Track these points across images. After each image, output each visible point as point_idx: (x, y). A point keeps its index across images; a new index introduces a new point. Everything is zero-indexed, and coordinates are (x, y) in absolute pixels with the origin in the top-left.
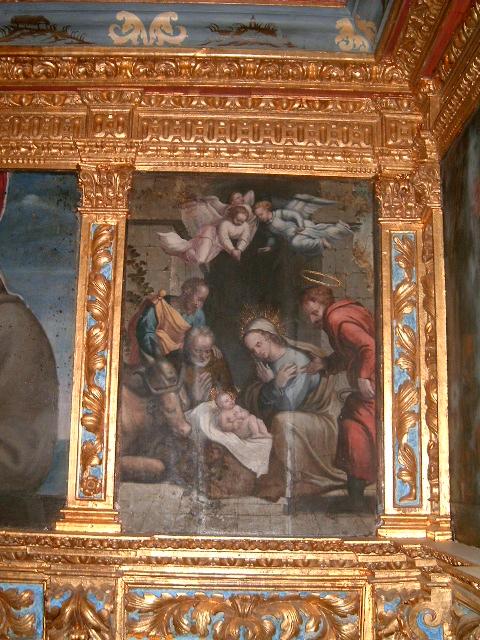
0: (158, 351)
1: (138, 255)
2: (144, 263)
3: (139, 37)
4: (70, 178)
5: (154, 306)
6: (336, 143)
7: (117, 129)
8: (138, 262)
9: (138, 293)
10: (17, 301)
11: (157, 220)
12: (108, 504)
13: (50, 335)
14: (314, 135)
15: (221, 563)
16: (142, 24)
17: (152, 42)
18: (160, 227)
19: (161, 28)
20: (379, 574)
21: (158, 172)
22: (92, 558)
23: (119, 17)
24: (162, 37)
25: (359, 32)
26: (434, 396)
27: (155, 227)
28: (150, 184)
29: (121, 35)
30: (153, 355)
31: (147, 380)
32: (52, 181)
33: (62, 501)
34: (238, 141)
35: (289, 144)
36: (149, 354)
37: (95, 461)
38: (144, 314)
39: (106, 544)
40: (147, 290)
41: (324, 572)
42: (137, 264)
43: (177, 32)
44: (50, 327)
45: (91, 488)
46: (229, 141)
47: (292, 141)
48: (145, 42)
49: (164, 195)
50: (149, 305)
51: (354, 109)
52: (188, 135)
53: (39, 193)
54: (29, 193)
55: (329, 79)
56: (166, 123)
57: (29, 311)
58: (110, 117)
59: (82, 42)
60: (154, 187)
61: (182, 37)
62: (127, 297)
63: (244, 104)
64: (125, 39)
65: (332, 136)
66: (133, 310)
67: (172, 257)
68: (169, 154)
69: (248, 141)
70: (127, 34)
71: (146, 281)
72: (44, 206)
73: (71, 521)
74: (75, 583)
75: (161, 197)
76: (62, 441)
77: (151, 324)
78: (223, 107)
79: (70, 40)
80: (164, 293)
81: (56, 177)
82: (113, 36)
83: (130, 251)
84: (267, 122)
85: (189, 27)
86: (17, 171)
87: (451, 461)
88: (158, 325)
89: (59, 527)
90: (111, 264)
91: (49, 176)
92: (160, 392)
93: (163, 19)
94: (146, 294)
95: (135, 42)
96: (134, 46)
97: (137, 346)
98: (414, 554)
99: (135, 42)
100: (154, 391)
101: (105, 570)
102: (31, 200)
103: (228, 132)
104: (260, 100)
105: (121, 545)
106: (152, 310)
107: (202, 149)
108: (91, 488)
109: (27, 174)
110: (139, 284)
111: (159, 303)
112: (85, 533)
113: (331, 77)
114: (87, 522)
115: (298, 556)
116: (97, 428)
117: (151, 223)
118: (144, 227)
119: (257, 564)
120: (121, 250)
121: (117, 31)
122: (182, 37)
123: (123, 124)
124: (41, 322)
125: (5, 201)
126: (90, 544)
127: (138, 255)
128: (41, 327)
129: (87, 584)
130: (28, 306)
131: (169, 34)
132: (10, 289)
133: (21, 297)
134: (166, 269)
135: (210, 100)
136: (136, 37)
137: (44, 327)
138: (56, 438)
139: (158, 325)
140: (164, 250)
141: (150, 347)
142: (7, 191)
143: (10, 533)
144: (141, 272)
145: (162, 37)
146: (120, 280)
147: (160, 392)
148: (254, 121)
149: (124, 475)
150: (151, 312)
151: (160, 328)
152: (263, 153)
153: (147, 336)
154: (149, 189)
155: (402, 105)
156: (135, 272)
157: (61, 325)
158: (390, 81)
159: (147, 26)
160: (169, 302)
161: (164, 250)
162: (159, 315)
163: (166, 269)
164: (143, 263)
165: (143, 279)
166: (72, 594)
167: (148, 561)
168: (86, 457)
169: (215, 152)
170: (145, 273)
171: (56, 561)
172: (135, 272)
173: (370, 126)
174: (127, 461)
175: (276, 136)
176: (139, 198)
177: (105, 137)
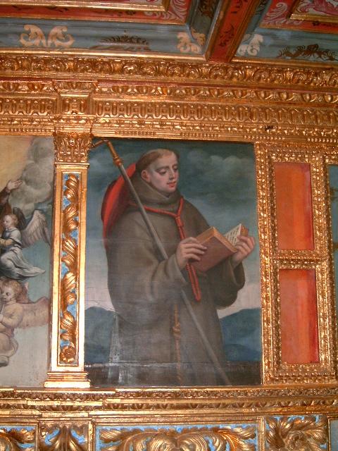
6: (8, 112)
14: (152, 111)
16: (42, 33)
23: (26, 28)
25: (194, 41)
34: (17, 113)
35: (164, 118)
43: (67, 39)
46: (11, 113)
47: (166, 116)
51: (242, 96)
56: (178, 106)
61: (69, 43)
65: (120, 110)
69: (109, 115)
82: (22, 41)
84: (107, 102)
104: (43, 85)
105: (87, 397)
112: (58, 389)
121: (25, 38)
129: (272, 384)
152: (123, 124)
166: (60, 431)
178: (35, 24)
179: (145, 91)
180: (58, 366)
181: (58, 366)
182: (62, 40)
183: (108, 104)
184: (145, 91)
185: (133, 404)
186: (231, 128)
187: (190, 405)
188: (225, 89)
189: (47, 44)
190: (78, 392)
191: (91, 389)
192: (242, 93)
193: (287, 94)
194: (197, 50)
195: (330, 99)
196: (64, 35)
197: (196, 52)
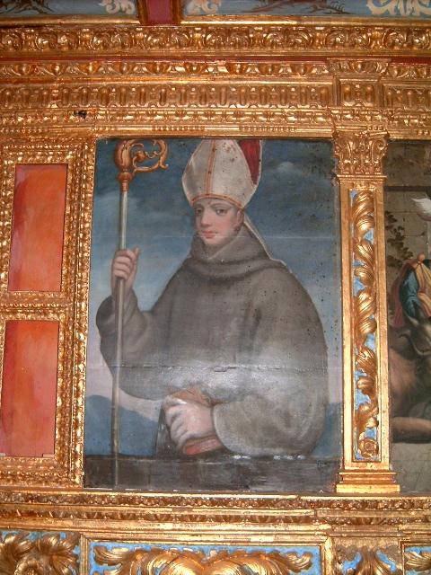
0: (422, 314)
1: (395, 221)
2: (403, 229)
3: (396, 7)
4: (324, 146)
5: (414, 270)
7: (366, 99)
8: (396, 227)
9: (398, 258)
10: (279, 267)
11: (410, 187)
12: (385, 464)
13: (315, 300)
17: (408, 13)
18: (415, 193)
21: (408, 140)
27: (409, 193)
28: (400, 151)
30: (417, 317)
31: (414, 344)
32: (304, 149)
33: (337, 463)
36: (413, 317)
37: (371, 423)
38: (406, 277)
39: (350, 505)
40: (407, 255)
42: (395, 230)
44: (314, 292)
45: (370, 449)
48: (402, 12)
49: (415, 163)
50: (410, 270)
52: (183, 101)
53: (294, 161)
54: (286, 160)
57: (292, 276)
58: (313, 90)
59: (340, 12)
60: (405, 154)
62: (391, 262)
63: (230, 68)
64: (382, 10)
66: (396, 274)
67: (428, 222)
68: (177, 118)
69: (216, 105)
71: (404, 246)
72: (300, 173)
73: (348, 483)
74: (360, 544)
75: (412, 164)
76: (333, 405)
77: (412, 287)
78: (132, 72)
79: (328, 10)
80: (423, 257)
81: (308, 145)
83: (389, 217)
86: (270, 139)
88: (420, 289)
89: (341, 489)
90: (372, 230)
91: (302, 144)
92: (425, 354)
94: (406, 259)
95: (393, 13)
96: (391, 17)
97: (401, 310)
99: (393, 13)
100: (420, 353)
101: (388, 530)
102: (285, 167)
106: (412, 274)
107: (181, 114)
108: (370, 449)
109: (279, 142)
110: (399, 249)
111: (419, 267)
114: (365, 484)
116: (370, 390)
117: (405, 189)
118: (398, 193)
120: (381, 215)
123: (372, 94)
124: (305, 287)
125: (260, 169)
126: (380, 505)
127: (395, 221)
128: (305, 292)
130: (291, 272)
131: (425, 6)
132: (273, 255)
133: (283, 262)
134: (423, 234)
135: (264, 68)
136: (393, 8)
137: (309, 291)
138: (328, 402)
139: (420, 289)
140: (419, 215)
141: (413, 310)
142: (261, 158)
143: (184, 495)
144: (400, 238)
146: (383, 245)
147: (425, 354)
148: (280, 87)
149: (397, 436)
150: (412, 276)
151: (423, 291)
152: (212, 116)
153: (410, 300)
154: (400, 157)
155: (356, 67)
156: (394, 237)
157: (325, 289)
160: (428, 266)
161: (419, 215)
162: (419, 279)
163: (423, 234)
164: (400, 228)
165: (402, 244)
167: (147, 518)
168: (360, 421)
169: (222, 115)
170: (403, 237)
171: (342, 523)
172: (394, 237)
174: (399, 421)
176: (391, 165)
177: (354, 106)
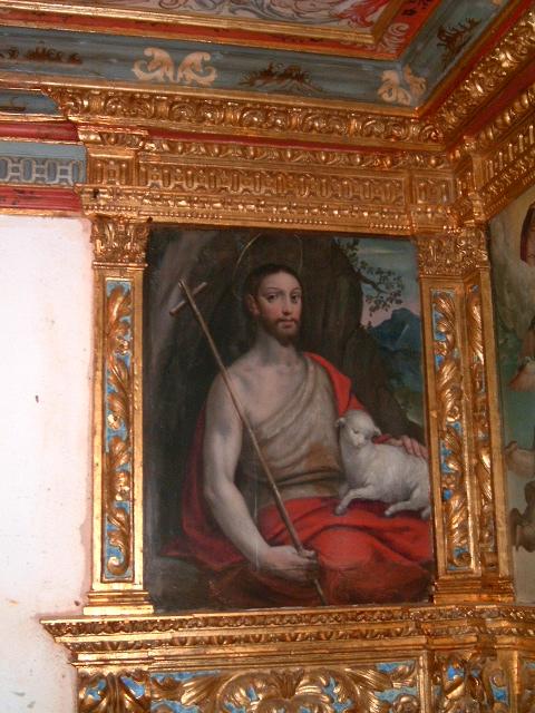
12: (98, 586)
15: (220, 642)
16: (170, 61)
17: (178, 80)
19: (192, 66)
20: (81, 657)
22: (194, 638)
24: (191, 76)
25: (405, 86)
26: (474, 461)
29: (147, 72)
41: (202, 651)
43: (208, 73)
48: (171, 79)
52: (190, 182)
55: (178, 120)
70: (153, 71)
82: (137, 71)
85: (220, 68)
87: (145, 535)
93: (195, 58)
98: (484, 616)
103: (117, 175)
113: (252, 124)
115: (167, 635)
119: (172, 643)
121: (144, 68)
122: (213, 77)
145: (191, 76)
158: (369, 135)
159: (177, 65)
173: (127, 161)
175: (49, 175)
178: (161, 48)
179: (180, 148)
180: (102, 581)
181: (102, 581)
182: (197, 73)
183: (178, 171)
184: (180, 148)
185: (210, 637)
186: (339, 210)
187: (176, 641)
188: (336, 152)
189: (175, 78)
190: (67, 622)
191: (155, 614)
192: (255, 152)
193: (362, 159)
194: (407, 99)
195: (323, 158)
196: (204, 64)
197: (405, 102)
